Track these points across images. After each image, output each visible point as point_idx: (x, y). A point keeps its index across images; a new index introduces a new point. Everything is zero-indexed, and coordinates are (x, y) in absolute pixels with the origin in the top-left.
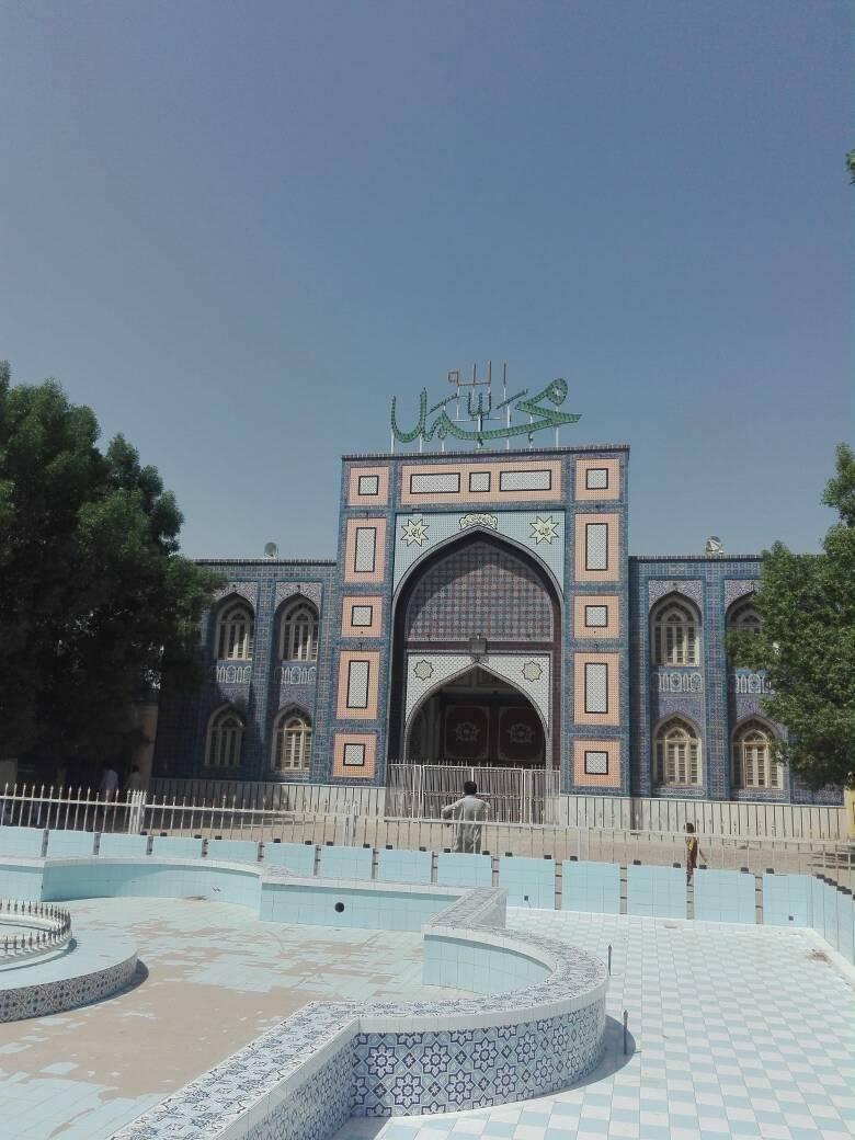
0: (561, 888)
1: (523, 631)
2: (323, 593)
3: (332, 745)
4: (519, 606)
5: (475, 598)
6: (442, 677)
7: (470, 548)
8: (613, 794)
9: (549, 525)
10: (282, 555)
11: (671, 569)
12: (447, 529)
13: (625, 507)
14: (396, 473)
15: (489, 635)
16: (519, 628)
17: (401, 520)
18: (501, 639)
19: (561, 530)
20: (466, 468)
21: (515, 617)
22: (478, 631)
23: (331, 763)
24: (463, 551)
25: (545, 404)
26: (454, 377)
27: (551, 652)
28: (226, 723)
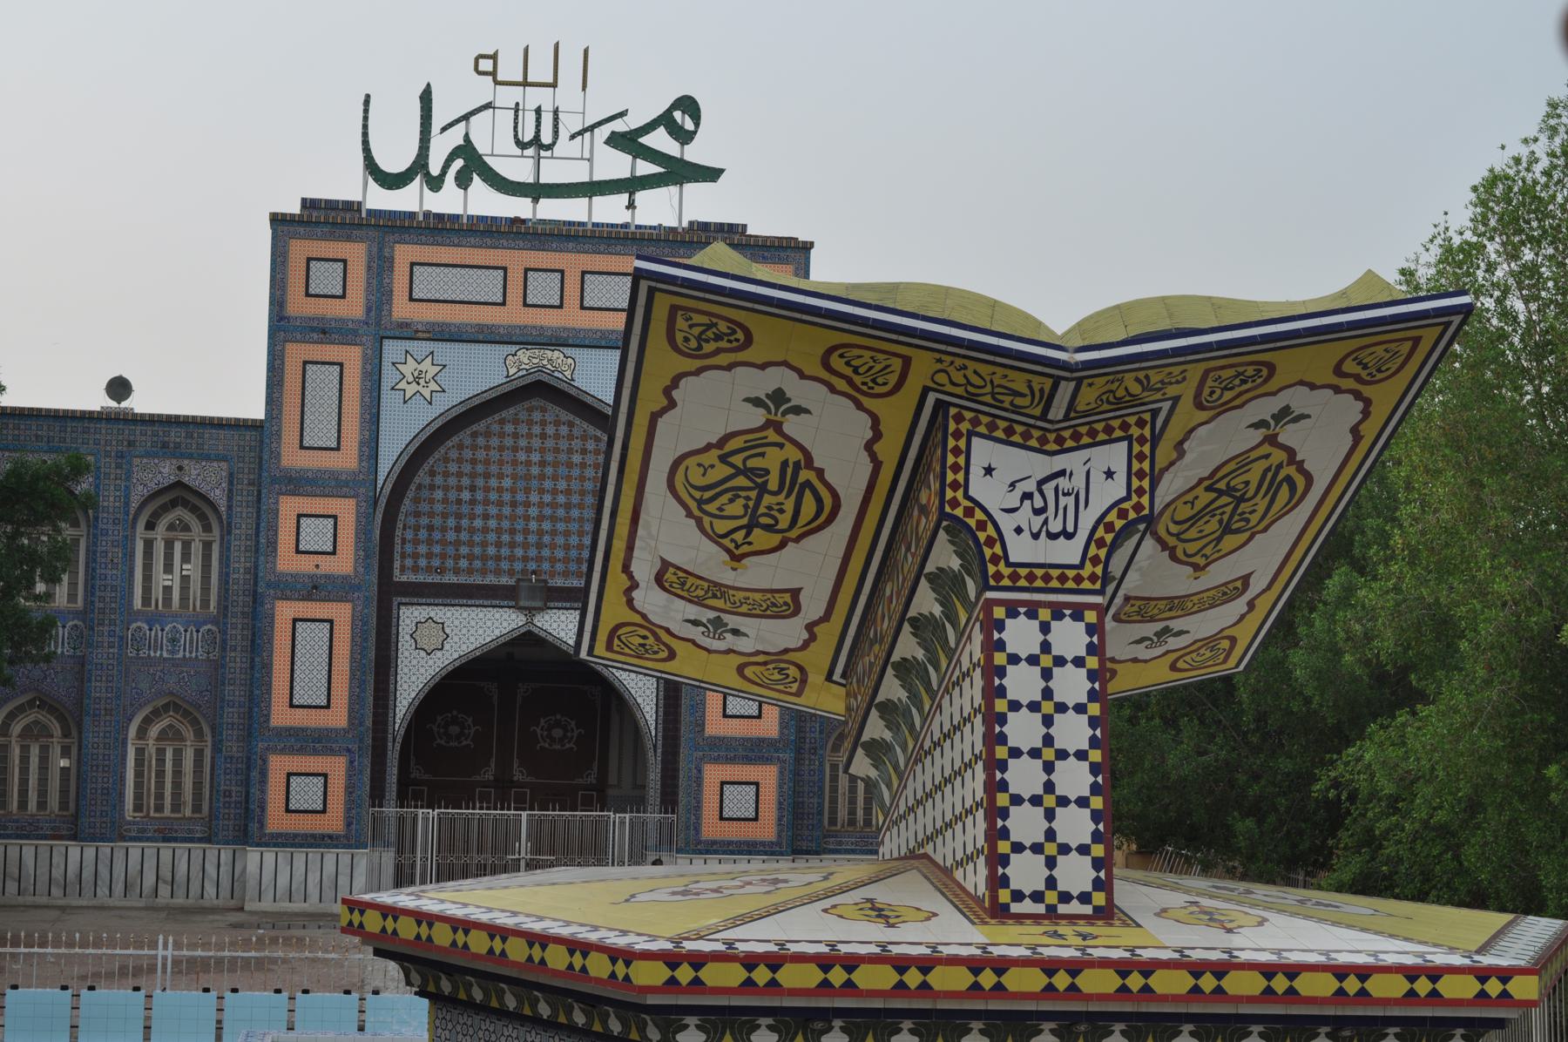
2: (231, 483)
5: (527, 504)
6: (465, 649)
7: (518, 410)
8: (765, 853)
10: (138, 404)
12: (481, 371)
14: (381, 257)
15: (552, 575)
17: (392, 350)
20: (518, 259)
22: (532, 566)
24: (504, 414)
25: (660, 140)
28: (163, 732)
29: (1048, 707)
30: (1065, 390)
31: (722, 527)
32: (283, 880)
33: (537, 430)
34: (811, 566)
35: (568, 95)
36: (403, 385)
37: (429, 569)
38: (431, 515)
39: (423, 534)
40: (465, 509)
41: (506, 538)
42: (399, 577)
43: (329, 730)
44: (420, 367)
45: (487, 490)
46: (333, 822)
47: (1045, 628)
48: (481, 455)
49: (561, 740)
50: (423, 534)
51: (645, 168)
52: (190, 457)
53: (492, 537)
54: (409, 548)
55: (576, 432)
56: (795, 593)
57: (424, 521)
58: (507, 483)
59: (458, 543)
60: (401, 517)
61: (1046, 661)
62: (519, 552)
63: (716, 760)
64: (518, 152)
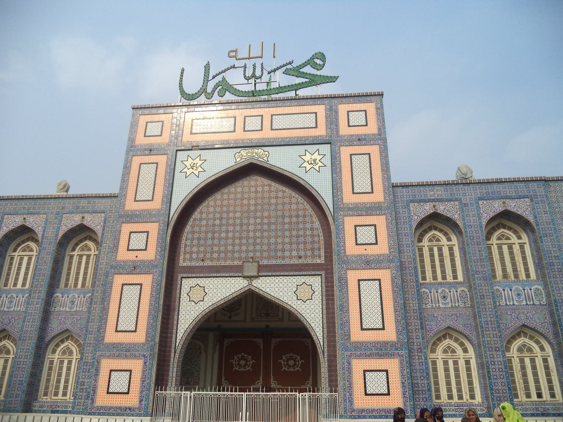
1: (294, 253)
2: (105, 223)
3: (97, 370)
4: (290, 230)
6: (215, 300)
9: (316, 156)
11: (430, 193)
13: (385, 141)
16: (291, 250)
18: (274, 262)
19: (327, 160)
21: (287, 240)
23: (95, 391)
25: (308, 69)
26: (233, 54)
27: (323, 273)
33: (253, 189)
36: (186, 170)
37: (197, 259)
38: (200, 232)
39: (195, 242)
40: (217, 229)
41: (237, 241)
43: (135, 344)
44: (194, 162)
45: (228, 219)
46: (132, 400)
48: (225, 203)
49: (293, 366)
50: (195, 242)
52: (88, 212)
53: (230, 241)
54: (188, 249)
55: (272, 189)
57: (196, 235)
58: (238, 215)
59: (213, 245)
60: (185, 234)
62: (244, 248)
63: (359, 357)
64: (246, 81)
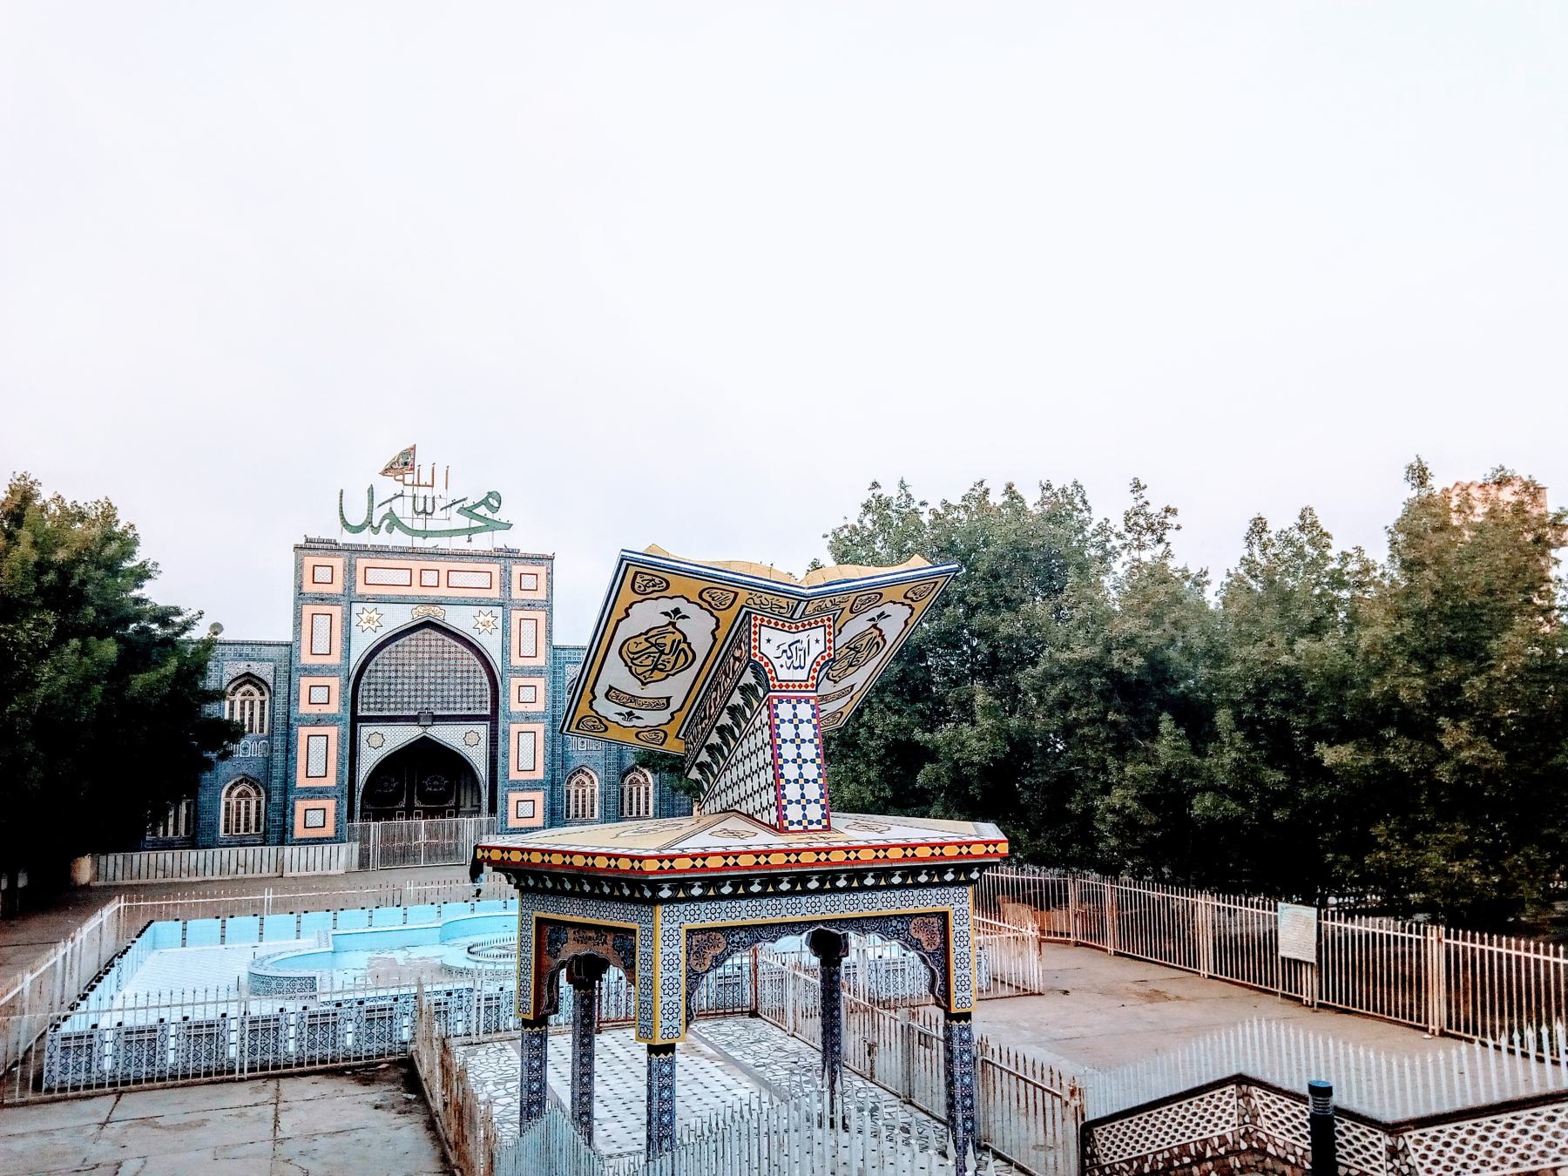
0: (487, 898)
12: (401, 617)
17: (356, 608)
20: (416, 565)
29: (797, 741)
30: (803, 604)
31: (640, 670)
32: (303, 862)
34: (677, 687)
35: (439, 488)
42: (360, 713)
46: (329, 831)
47: (794, 707)
51: (475, 523)
56: (668, 699)
61: (796, 722)
